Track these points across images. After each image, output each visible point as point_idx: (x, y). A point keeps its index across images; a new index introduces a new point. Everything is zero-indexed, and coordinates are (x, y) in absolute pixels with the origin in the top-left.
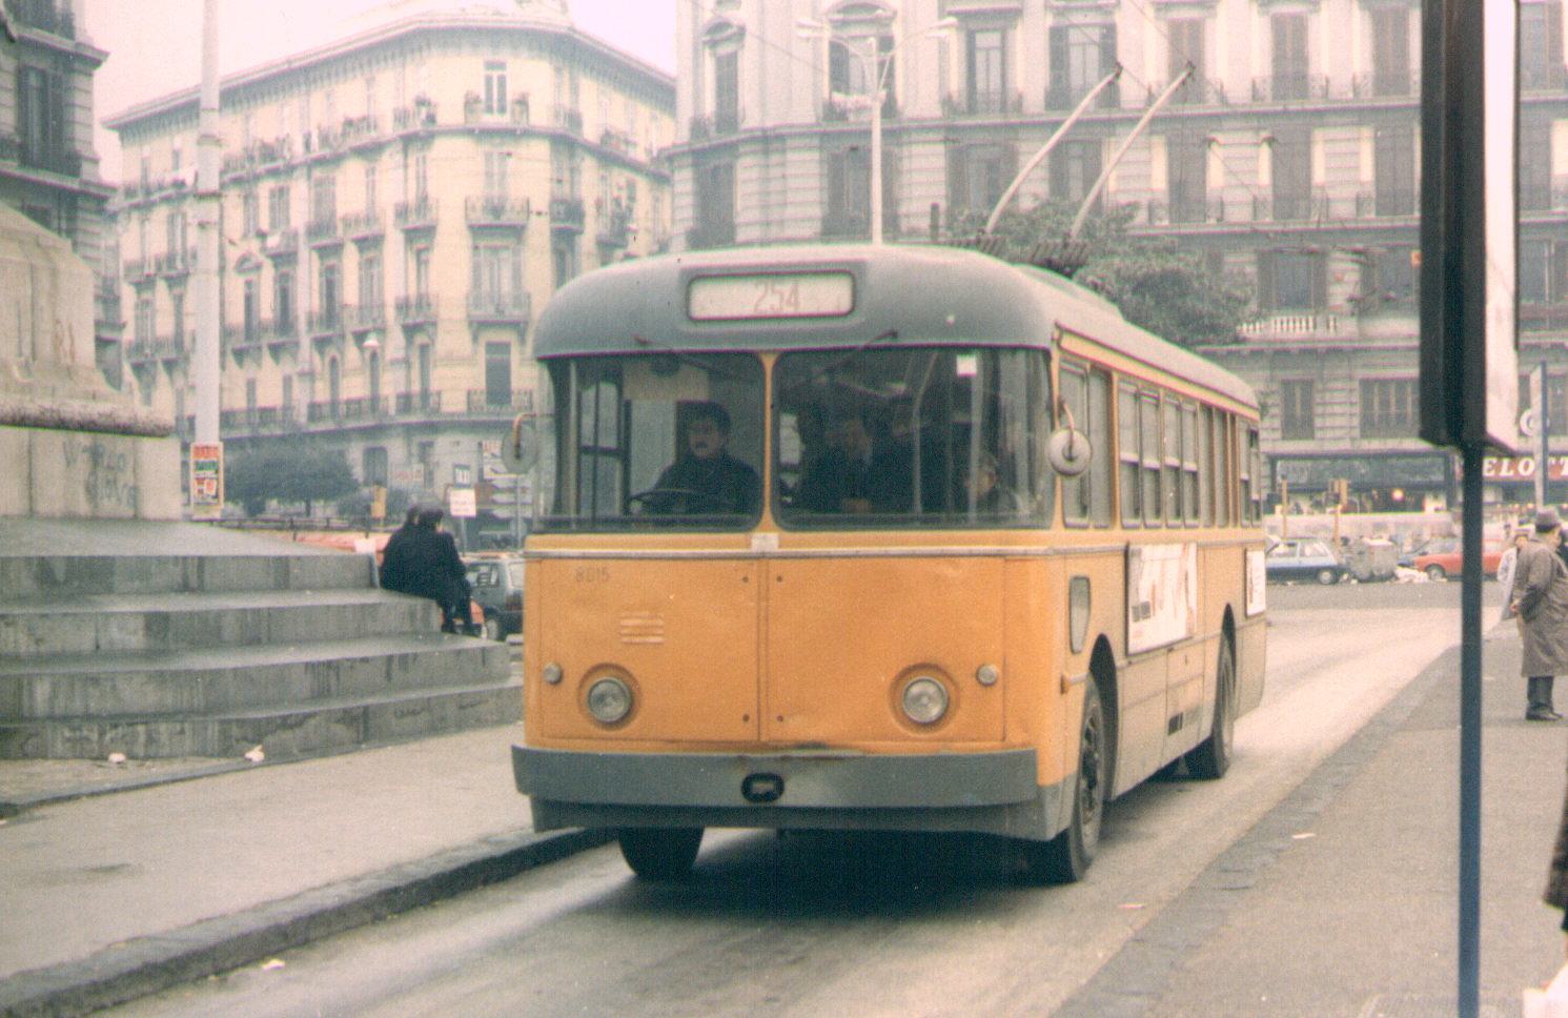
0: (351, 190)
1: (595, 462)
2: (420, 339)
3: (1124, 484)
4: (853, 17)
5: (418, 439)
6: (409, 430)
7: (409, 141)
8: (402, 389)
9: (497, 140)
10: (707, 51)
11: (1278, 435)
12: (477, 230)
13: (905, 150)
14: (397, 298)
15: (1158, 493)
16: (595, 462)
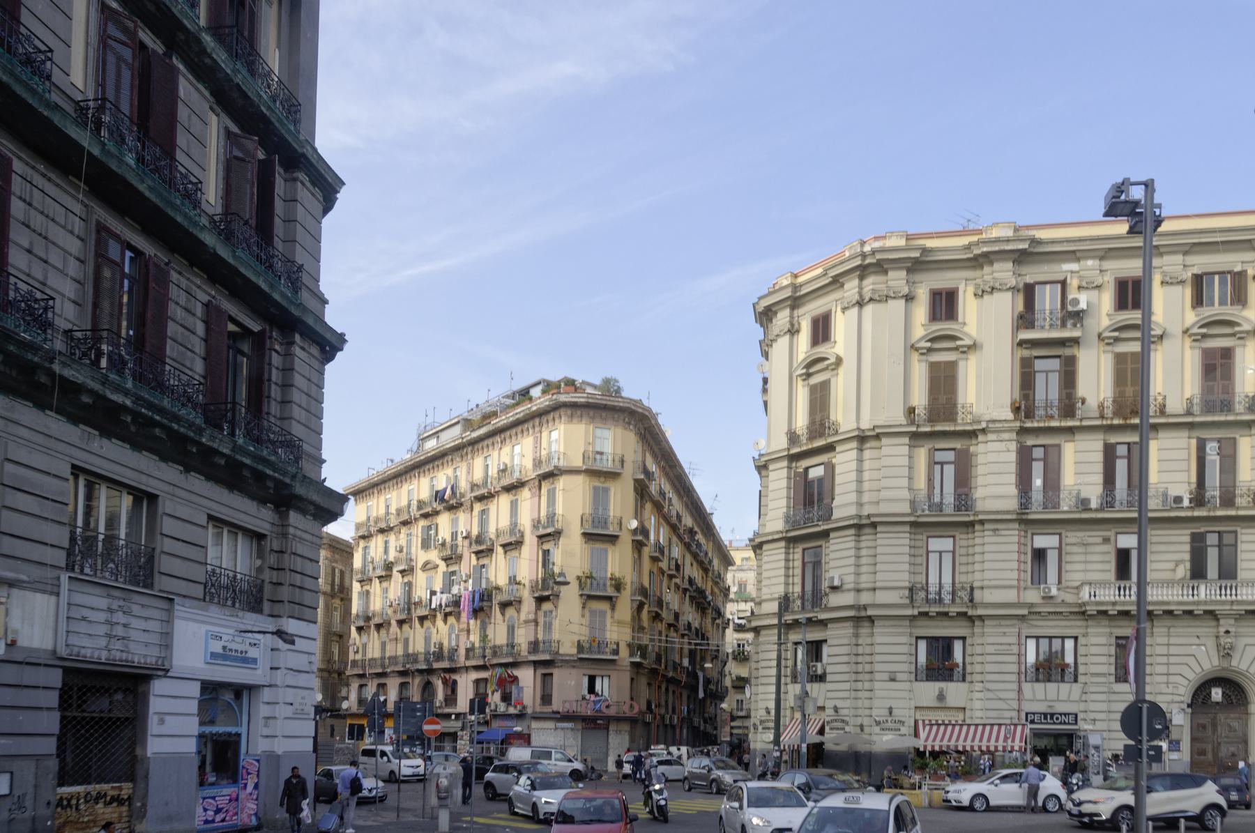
0: (499, 514)
1: (1011, 587)
2: (547, 606)
3: (543, 738)
4: (937, 346)
5: (541, 671)
6: (536, 664)
7: (507, 547)
8: (532, 639)
9: (602, 479)
10: (800, 383)
11: (1112, 679)
12: (588, 537)
13: (981, 448)
14: (531, 581)
15: (739, 727)
16: (1011, 587)
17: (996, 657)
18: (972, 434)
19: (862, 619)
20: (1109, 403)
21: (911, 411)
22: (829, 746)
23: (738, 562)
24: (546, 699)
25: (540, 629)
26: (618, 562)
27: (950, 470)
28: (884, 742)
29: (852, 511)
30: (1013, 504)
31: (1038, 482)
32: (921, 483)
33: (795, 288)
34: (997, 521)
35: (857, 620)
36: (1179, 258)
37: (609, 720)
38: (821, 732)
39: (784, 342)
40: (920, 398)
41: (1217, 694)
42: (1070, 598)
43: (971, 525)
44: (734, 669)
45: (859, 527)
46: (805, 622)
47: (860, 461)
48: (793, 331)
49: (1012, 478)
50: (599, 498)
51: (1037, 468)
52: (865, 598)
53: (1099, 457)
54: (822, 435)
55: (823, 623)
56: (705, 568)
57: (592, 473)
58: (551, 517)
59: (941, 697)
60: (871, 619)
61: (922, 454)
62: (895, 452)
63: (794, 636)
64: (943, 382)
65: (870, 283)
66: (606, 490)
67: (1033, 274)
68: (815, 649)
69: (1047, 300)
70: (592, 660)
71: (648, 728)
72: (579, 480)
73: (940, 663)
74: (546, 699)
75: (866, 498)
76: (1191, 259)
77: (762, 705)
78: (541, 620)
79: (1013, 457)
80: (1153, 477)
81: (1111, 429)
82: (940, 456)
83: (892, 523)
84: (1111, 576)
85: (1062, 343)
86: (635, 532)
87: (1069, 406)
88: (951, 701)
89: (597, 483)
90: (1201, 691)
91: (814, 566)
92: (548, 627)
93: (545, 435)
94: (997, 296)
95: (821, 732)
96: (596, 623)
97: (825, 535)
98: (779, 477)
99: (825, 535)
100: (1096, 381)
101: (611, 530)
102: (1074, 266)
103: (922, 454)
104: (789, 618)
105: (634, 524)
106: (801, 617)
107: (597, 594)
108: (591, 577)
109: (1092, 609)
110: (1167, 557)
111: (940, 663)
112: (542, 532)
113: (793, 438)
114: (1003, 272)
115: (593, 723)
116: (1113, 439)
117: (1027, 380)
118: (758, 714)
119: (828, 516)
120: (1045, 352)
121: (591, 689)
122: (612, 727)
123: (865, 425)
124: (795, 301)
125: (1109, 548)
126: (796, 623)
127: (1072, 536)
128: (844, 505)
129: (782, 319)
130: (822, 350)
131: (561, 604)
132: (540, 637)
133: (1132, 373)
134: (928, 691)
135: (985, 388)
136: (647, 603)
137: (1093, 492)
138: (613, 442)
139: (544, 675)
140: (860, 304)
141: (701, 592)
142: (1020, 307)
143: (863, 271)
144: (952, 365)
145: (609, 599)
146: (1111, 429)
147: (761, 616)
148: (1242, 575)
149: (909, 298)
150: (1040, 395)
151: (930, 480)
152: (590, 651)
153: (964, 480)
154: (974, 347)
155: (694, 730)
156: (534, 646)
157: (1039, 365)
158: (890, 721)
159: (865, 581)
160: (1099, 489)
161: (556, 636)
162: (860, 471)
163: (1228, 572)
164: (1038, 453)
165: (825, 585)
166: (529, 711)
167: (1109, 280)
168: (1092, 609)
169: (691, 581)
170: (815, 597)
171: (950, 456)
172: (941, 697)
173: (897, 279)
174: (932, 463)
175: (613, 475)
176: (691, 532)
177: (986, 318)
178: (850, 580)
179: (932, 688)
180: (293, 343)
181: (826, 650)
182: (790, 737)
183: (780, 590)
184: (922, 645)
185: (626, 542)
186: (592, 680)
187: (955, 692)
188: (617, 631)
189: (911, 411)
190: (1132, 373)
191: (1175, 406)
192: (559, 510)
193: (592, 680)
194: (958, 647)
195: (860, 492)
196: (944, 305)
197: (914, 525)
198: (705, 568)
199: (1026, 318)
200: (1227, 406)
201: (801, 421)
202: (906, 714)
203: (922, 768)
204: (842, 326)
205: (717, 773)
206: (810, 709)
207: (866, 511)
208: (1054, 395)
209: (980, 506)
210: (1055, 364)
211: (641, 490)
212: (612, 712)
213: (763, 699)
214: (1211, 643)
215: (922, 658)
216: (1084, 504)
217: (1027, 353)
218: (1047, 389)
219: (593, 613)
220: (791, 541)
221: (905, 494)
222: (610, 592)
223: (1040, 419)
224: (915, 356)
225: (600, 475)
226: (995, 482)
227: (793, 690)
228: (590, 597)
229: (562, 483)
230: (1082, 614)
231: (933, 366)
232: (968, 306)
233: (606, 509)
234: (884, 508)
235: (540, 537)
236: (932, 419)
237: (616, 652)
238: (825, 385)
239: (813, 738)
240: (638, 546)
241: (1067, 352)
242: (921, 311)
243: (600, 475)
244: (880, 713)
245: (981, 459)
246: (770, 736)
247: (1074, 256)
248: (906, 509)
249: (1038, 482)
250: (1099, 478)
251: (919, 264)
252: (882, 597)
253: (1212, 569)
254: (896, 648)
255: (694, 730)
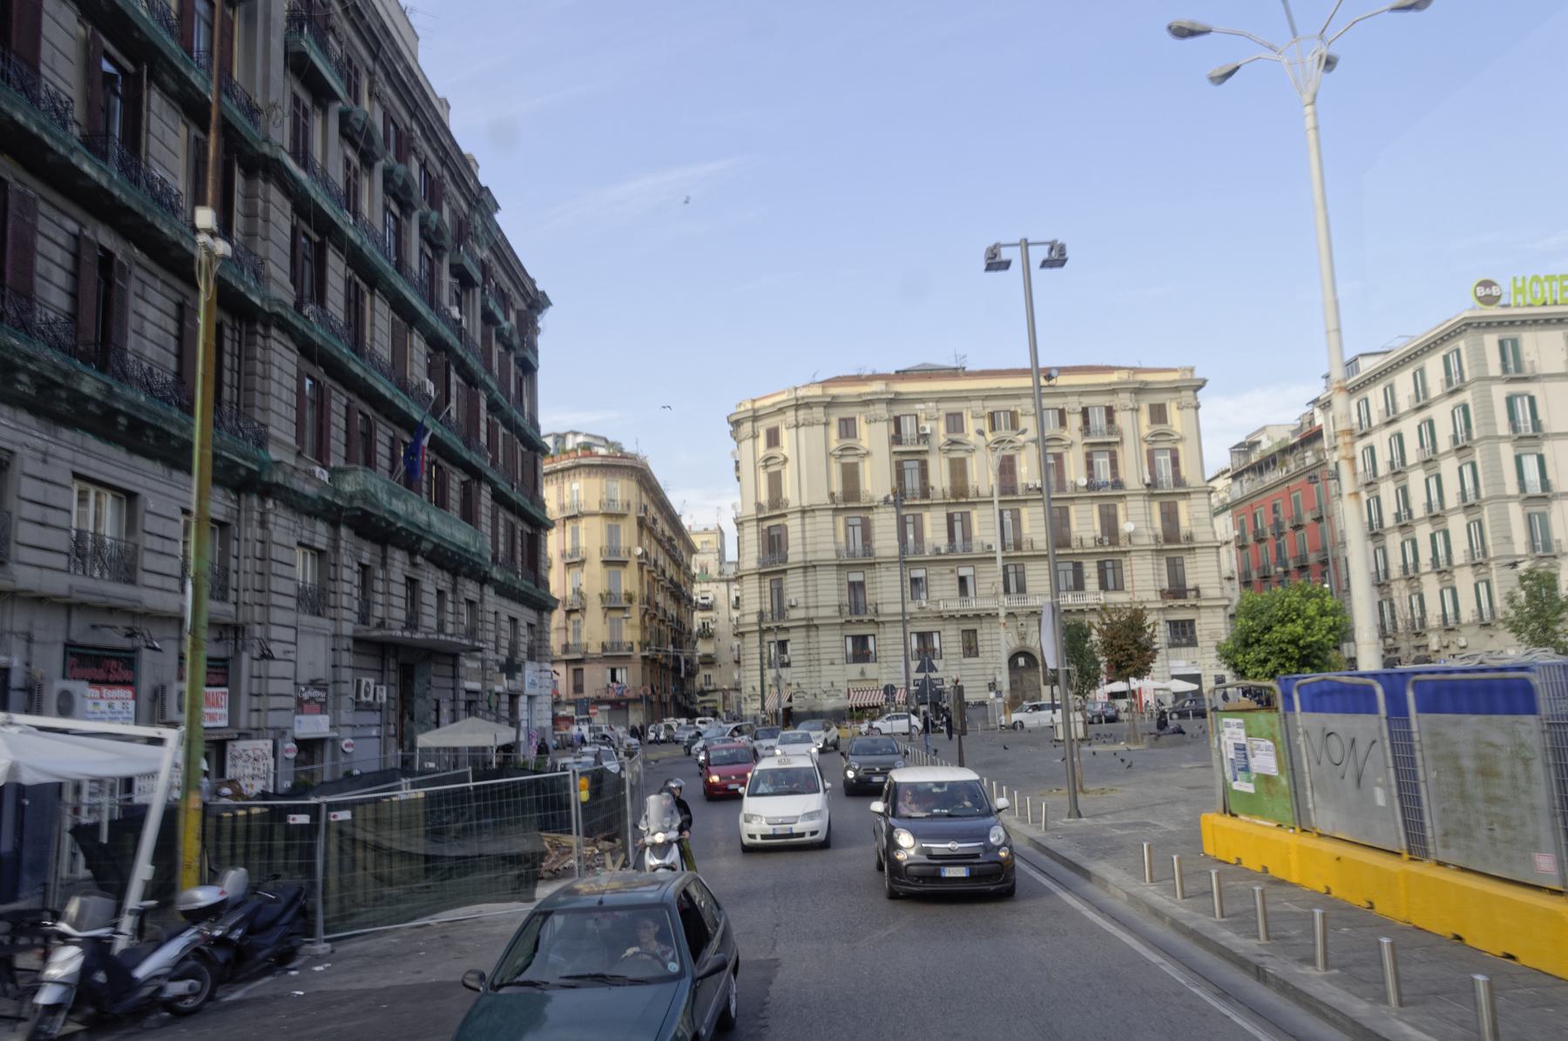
2: (574, 617)
6: (568, 662)
12: (606, 563)
17: (891, 646)
18: (870, 508)
19: (810, 626)
20: (948, 490)
21: (832, 495)
22: (796, 709)
23: (698, 546)
24: (578, 688)
25: (570, 634)
26: (629, 581)
27: (858, 530)
28: (829, 703)
29: (800, 558)
30: (896, 552)
31: (911, 537)
32: (841, 538)
33: (755, 411)
34: (888, 563)
35: (808, 627)
36: (980, 403)
37: (628, 701)
38: (790, 700)
39: (748, 443)
40: (837, 487)
41: (1021, 661)
42: (934, 608)
43: (873, 564)
44: (703, 648)
45: (805, 568)
46: (775, 628)
47: (803, 525)
48: (755, 436)
49: (895, 535)
50: (613, 533)
51: (910, 528)
52: (812, 613)
53: (945, 521)
54: (777, 507)
55: (787, 629)
56: (677, 563)
57: (607, 515)
58: (576, 550)
59: (862, 673)
60: (816, 626)
61: (841, 520)
62: (824, 520)
63: (768, 638)
64: (851, 475)
65: (802, 414)
66: (618, 527)
67: (898, 410)
68: (782, 645)
69: (908, 428)
70: (613, 656)
71: (657, 709)
72: (597, 520)
73: (861, 652)
74: (578, 688)
75: (808, 548)
76: (987, 403)
77: (749, 684)
78: (571, 627)
79: (894, 522)
80: (976, 531)
81: (949, 504)
82: (851, 521)
83: (825, 565)
84: (957, 593)
85: (919, 452)
86: (639, 557)
87: (925, 492)
88: (869, 675)
89: (610, 522)
90: (1013, 660)
91: (778, 593)
92: (577, 632)
93: (567, 485)
94: (879, 424)
95: (790, 700)
96: (615, 628)
97: (784, 571)
98: (751, 533)
99: (784, 571)
100: (939, 477)
101: (623, 557)
102: (922, 406)
103: (841, 520)
104: (764, 626)
105: (639, 551)
106: (772, 625)
107: (613, 605)
108: (609, 594)
109: (946, 615)
110: (988, 580)
111: (861, 652)
112: (569, 560)
113: (759, 507)
114: (881, 410)
115: (619, 705)
116: (951, 510)
117: (900, 474)
118: (747, 690)
119: (785, 561)
120: (909, 461)
121: (613, 679)
122: (631, 707)
123: (805, 503)
124: (755, 418)
125: (954, 576)
126: (769, 629)
127: (933, 570)
128: (795, 554)
129: (747, 428)
130: (774, 451)
131: (587, 615)
132: (571, 641)
133: (958, 469)
134: (855, 669)
135: (876, 480)
136: (650, 611)
137: (942, 542)
138: (623, 490)
139: (575, 671)
140: (797, 426)
141: (678, 586)
142: (893, 431)
143: (797, 407)
144: (856, 465)
145: (623, 609)
146: (949, 504)
147: (745, 625)
148: (1029, 589)
149: (827, 424)
150: (908, 485)
151: (847, 536)
152: (612, 649)
153: (867, 537)
154: (868, 454)
155: (678, 705)
156: (566, 648)
157: (906, 465)
158: (832, 690)
159: (811, 601)
160: (946, 541)
161: (584, 640)
162: (803, 531)
163: (1021, 589)
164: (910, 519)
165: (786, 604)
166: (563, 699)
167: (942, 414)
168: (946, 615)
169: (671, 581)
170: (780, 612)
171: (858, 521)
172: (862, 673)
173: (818, 413)
174: (847, 526)
175: (622, 516)
176: (670, 539)
177: (872, 436)
178: (802, 602)
179: (858, 667)
180: (255, 344)
181: (789, 646)
182: (771, 704)
183: (757, 608)
184: (849, 641)
185: (634, 563)
186: (613, 672)
187: (870, 669)
188: (631, 634)
189: (832, 495)
190: (958, 469)
191: (985, 490)
192: (583, 543)
193: (613, 672)
194: (871, 641)
195: (804, 545)
196: (848, 428)
197: (839, 566)
198: (677, 563)
199: (897, 439)
200: (1014, 491)
201: (764, 497)
202: (841, 685)
203: (852, 718)
204: (786, 437)
205: (1094, 632)
206: (783, 686)
207: (810, 557)
208: (917, 485)
209: (877, 553)
210: (916, 464)
211: (641, 523)
212: (631, 695)
213: (751, 683)
214: (1014, 631)
215: (850, 649)
216: (937, 551)
217: (899, 458)
218: (913, 482)
219: (612, 620)
220: (762, 575)
221: (832, 546)
222: (624, 604)
223: (908, 496)
224: (833, 460)
225: (612, 516)
226: (885, 540)
227: (770, 674)
228: (610, 609)
229: (583, 524)
230: (940, 617)
231: (844, 466)
232: (863, 429)
233: (618, 541)
234: (820, 556)
235: (568, 564)
236: (845, 500)
237: (631, 649)
238: (778, 474)
239: (786, 704)
240: (641, 566)
241: (922, 457)
242: (834, 432)
243: (612, 516)
244: (825, 686)
245: (876, 524)
246: (758, 705)
247: (921, 401)
248: (833, 555)
249: (911, 537)
250: (945, 534)
251: (831, 404)
252: (822, 612)
253: (1013, 588)
254: (833, 644)
255: (678, 705)
